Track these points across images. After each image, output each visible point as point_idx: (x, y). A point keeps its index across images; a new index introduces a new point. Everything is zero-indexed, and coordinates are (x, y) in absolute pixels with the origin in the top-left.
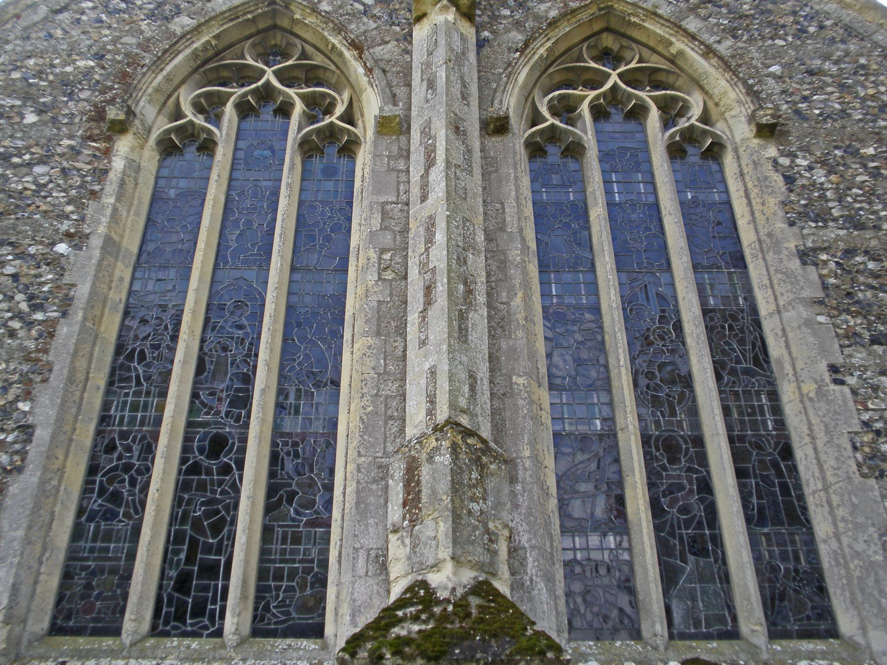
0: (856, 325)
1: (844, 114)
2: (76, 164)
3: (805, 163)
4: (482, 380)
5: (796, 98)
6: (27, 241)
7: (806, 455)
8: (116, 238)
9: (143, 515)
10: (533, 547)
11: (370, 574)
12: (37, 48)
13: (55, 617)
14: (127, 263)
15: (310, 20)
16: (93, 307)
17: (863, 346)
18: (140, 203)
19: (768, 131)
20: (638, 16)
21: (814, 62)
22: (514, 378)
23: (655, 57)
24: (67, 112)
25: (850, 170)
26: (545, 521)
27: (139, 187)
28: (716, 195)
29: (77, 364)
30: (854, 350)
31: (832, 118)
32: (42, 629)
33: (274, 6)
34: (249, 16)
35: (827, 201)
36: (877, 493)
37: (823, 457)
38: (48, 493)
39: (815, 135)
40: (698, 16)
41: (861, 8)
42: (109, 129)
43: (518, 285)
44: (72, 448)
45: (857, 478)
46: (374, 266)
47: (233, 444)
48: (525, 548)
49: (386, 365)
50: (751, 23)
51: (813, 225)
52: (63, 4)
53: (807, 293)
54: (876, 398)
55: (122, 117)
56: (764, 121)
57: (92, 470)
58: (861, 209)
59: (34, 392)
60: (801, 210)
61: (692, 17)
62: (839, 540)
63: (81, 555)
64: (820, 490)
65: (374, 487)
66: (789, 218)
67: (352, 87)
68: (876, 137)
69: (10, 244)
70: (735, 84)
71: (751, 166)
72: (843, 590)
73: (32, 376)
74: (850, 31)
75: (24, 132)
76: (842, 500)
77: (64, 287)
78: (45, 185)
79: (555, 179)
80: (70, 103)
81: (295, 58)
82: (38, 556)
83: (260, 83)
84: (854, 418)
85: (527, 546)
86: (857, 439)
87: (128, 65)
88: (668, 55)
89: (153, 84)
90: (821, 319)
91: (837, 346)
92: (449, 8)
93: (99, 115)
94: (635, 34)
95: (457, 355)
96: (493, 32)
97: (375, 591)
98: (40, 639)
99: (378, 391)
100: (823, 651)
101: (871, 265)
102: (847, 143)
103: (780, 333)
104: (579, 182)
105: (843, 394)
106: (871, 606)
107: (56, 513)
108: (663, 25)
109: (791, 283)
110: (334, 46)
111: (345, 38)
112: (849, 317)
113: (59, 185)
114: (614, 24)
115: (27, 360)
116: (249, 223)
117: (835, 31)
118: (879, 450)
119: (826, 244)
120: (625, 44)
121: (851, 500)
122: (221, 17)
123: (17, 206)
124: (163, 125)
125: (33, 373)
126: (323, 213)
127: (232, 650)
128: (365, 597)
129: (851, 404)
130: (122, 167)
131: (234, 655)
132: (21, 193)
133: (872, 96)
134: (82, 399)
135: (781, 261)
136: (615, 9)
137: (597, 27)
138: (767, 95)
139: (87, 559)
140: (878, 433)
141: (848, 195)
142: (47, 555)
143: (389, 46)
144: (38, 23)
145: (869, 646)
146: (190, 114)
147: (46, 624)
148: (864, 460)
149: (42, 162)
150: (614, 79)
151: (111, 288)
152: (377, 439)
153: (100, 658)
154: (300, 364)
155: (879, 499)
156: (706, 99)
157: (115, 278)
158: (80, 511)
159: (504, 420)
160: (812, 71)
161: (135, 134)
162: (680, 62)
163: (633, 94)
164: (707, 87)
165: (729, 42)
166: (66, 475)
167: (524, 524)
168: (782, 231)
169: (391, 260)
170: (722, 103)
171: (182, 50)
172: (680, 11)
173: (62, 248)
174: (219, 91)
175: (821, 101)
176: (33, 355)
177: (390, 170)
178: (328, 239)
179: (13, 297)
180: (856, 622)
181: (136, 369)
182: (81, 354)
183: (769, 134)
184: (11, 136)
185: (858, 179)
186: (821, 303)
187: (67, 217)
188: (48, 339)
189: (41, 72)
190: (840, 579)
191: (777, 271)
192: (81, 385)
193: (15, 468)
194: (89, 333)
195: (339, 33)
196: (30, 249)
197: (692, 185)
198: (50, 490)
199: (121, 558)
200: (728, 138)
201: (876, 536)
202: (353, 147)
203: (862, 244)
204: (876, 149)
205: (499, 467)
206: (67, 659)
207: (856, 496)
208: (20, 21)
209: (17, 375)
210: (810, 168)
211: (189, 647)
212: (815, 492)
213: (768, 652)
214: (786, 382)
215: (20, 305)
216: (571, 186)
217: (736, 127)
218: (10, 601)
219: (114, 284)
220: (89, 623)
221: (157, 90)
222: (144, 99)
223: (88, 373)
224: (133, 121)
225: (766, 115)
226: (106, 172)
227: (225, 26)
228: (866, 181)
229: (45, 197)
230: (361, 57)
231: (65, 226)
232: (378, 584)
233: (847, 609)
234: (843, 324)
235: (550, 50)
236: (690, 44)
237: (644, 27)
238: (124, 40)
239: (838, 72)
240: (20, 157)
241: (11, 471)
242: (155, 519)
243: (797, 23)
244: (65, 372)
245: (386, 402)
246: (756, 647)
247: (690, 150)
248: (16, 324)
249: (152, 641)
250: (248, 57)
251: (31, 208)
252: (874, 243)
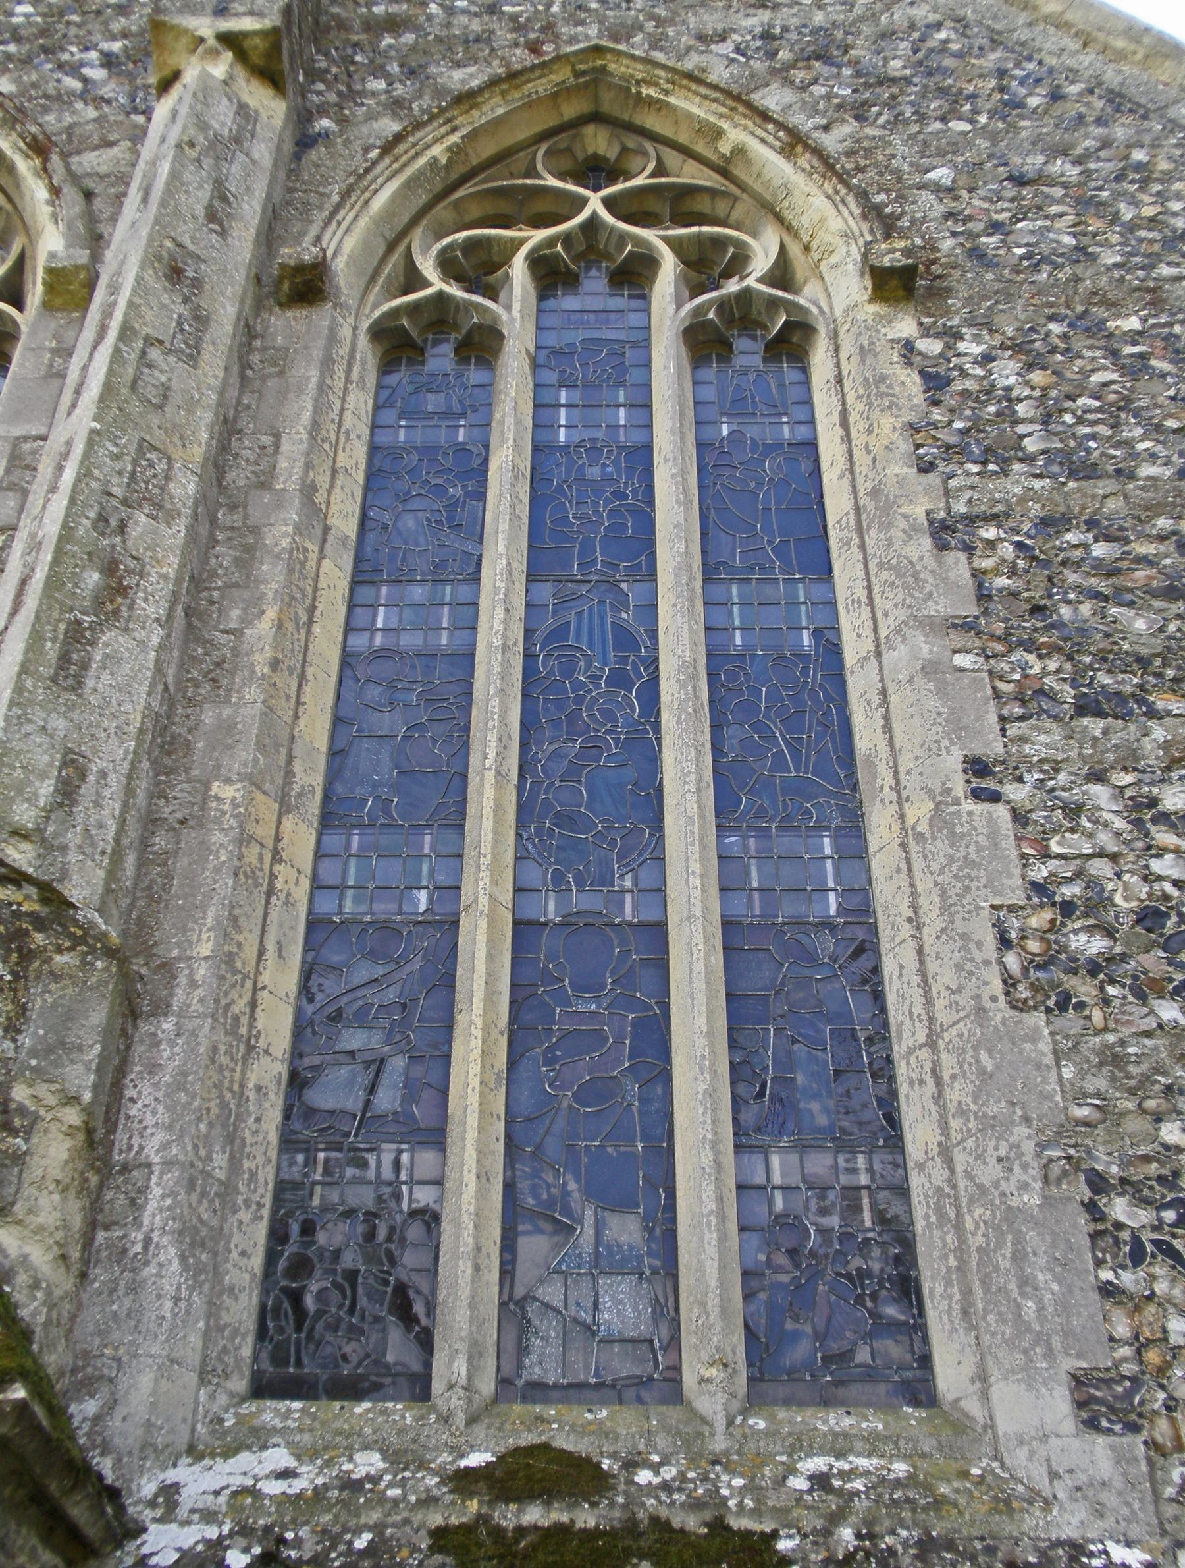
0: (1045, 673)
1: (1082, 254)
3: (977, 349)
4: (103, 774)
5: (978, 227)
7: (901, 967)
10: (168, 1164)
17: (1056, 718)
19: (895, 284)
20: (656, 85)
21: (1029, 160)
22: (215, 788)
23: (691, 166)
25: (1079, 362)
26: (224, 1105)
28: (786, 428)
30: (1033, 728)
31: (1052, 262)
35: (1017, 422)
36: (1045, 1046)
37: (932, 967)
39: (1010, 295)
40: (788, 82)
41: (1147, 57)
43: (270, 595)
45: (1001, 1011)
48: (149, 1165)
50: (902, 92)
51: (975, 469)
53: (940, 607)
54: (1072, 830)
56: (886, 262)
58: (1093, 437)
60: (953, 440)
61: (774, 86)
62: (949, 1162)
64: (921, 1046)
66: (920, 458)
68: (1148, 297)
70: (843, 201)
71: (856, 359)
72: (949, 1284)
74: (1117, 100)
76: (961, 1065)
79: (433, 402)
84: (1010, 875)
85: (157, 1160)
86: (1014, 925)
88: (714, 158)
90: (961, 660)
91: (993, 718)
92: (218, 53)
94: (651, 121)
95: (38, 716)
96: (343, 122)
100: (874, 1434)
101: (1100, 550)
102: (1080, 309)
103: (876, 700)
104: (480, 407)
105: (991, 820)
106: (1002, 1320)
108: (705, 97)
109: (906, 587)
111: (21, 136)
112: (1031, 658)
114: (609, 103)
117: (1088, 104)
118: (1064, 948)
119: (999, 508)
120: (631, 144)
121: (978, 1061)
129: (1008, 844)
133: (1152, 220)
135: (890, 543)
136: (611, 74)
137: (570, 110)
138: (913, 221)
140: (1067, 908)
141: (1065, 410)
145: (991, 1426)
146: (437, 283)
148: (1025, 970)
150: (595, 203)
155: (1049, 1060)
156: (788, 240)
159: (169, 877)
160: (1022, 176)
162: (738, 171)
163: (628, 234)
164: (787, 215)
165: (848, 127)
167: (161, 1109)
168: (901, 482)
170: (814, 245)
172: (752, 76)
175: (1033, 232)
180: (969, 1366)
183: (901, 293)
185: (1095, 378)
186: (967, 626)
190: (945, 1257)
191: (881, 566)
195: (13, 128)
197: (738, 407)
200: (822, 312)
201: (1029, 1147)
203: (1083, 508)
204: (1144, 320)
205: (84, 963)
207: (990, 1053)
210: (987, 359)
212: (911, 1051)
213: (729, 1434)
214: (878, 804)
216: (463, 415)
217: (837, 289)
225: (893, 251)
228: (1113, 382)
233: (954, 1330)
234: (1013, 670)
235: (455, 151)
236: (759, 132)
237: (668, 104)
239: (1082, 178)
243: (1002, 89)
246: (704, 1421)
247: (741, 344)
252: (1112, 505)
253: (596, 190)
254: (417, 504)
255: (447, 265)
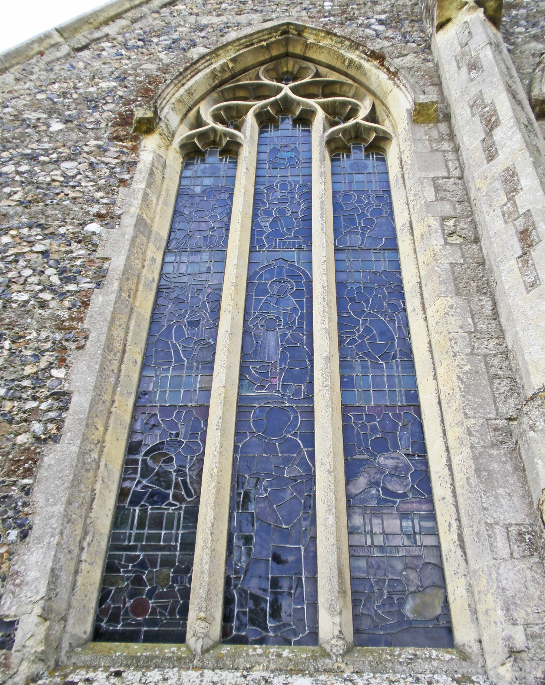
2: (104, 159)
6: (57, 223)
8: (148, 221)
9: (199, 497)
11: (515, 555)
12: (61, 76)
13: (98, 619)
14: (158, 246)
15: (326, 42)
16: (128, 279)
18: (168, 195)
24: (93, 120)
27: (166, 181)
29: (115, 333)
32: (85, 633)
33: (287, 35)
34: (264, 43)
38: (89, 466)
42: (135, 131)
44: (112, 421)
46: (437, 232)
47: (296, 418)
49: (475, 324)
52: (84, 44)
55: (150, 114)
57: (132, 448)
59: (68, 359)
63: (126, 543)
65: (494, 452)
67: (374, 94)
69: (39, 226)
73: (65, 343)
75: (51, 137)
77: (97, 261)
78: (73, 177)
80: (94, 114)
81: (310, 76)
82: (78, 539)
83: (279, 96)
87: (150, 83)
89: (176, 96)
93: (125, 120)
97: (529, 578)
98: (83, 644)
99: (473, 349)
107: (97, 492)
110: (351, 62)
111: (364, 52)
113: (87, 177)
115: (60, 329)
116: (282, 212)
122: (238, 43)
123: (45, 195)
124: (183, 132)
125: (67, 340)
126: (359, 201)
127: (340, 659)
128: (518, 586)
130: (151, 159)
131: (343, 666)
132: (49, 184)
134: (120, 371)
139: (133, 548)
142: (88, 539)
143: (408, 58)
144: (60, 58)
146: (211, 123)
147: (88, 627)
149: (68, 159)
151: (144, 266)
152: (484, 399)
153: (164, 668)
154: (360, 337)
157: (148, 258)
158: (122, 494)
161: (161, 134)
166: (105, 449)
169: (455, 226)
171: (202, 70)
173: (94, 227)
174: (237, 106)
176: (67, 324)
177: (433, 151)
178: (370, 221)
179: (43, 272)
181: (174, 345)
182: (118, 323)
184: (38, 141)
187: (98, 202)
188: (82, 309)
189: (64, 93)
192: (119, 355)
193: (49, 437)
194: (125, 305)
195: (357, 49)
196: (60, 229)
198: (90, 463)
199: (176, 546)
202: (382, 144)
206: (122, 669)
208: (44, 57)
209: (50, 343)
211: (279, 656)
215: (51, 279)
218: (49, 590)
219: (146, 263)
220: (143, 626)
221: (179, 101)
222: (167, 107)
223: (125, 345)
224: (158, 124)
226: (135, 163)
227: (241, 52)
229: (74, 187)
230: (382, 65)
231: (95, 209)
232: (531, 568)
238: (143, 67)
240: (48, 156)
241: (45, 440)
242: (217, 498)
244: (103, 338)
245: (485, 361)
248: (47, 296)
249: (226, 649)
250: (262, 78)
251: (60, 196)
253: (286, 84)
254: (196, 224)
255: (217, 118)
